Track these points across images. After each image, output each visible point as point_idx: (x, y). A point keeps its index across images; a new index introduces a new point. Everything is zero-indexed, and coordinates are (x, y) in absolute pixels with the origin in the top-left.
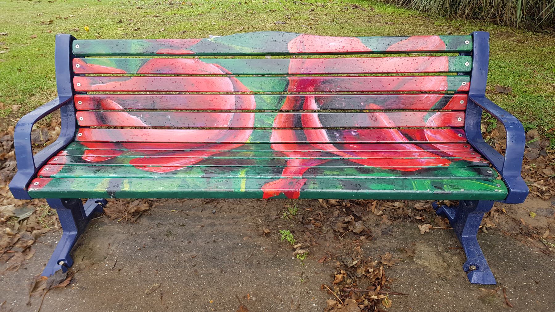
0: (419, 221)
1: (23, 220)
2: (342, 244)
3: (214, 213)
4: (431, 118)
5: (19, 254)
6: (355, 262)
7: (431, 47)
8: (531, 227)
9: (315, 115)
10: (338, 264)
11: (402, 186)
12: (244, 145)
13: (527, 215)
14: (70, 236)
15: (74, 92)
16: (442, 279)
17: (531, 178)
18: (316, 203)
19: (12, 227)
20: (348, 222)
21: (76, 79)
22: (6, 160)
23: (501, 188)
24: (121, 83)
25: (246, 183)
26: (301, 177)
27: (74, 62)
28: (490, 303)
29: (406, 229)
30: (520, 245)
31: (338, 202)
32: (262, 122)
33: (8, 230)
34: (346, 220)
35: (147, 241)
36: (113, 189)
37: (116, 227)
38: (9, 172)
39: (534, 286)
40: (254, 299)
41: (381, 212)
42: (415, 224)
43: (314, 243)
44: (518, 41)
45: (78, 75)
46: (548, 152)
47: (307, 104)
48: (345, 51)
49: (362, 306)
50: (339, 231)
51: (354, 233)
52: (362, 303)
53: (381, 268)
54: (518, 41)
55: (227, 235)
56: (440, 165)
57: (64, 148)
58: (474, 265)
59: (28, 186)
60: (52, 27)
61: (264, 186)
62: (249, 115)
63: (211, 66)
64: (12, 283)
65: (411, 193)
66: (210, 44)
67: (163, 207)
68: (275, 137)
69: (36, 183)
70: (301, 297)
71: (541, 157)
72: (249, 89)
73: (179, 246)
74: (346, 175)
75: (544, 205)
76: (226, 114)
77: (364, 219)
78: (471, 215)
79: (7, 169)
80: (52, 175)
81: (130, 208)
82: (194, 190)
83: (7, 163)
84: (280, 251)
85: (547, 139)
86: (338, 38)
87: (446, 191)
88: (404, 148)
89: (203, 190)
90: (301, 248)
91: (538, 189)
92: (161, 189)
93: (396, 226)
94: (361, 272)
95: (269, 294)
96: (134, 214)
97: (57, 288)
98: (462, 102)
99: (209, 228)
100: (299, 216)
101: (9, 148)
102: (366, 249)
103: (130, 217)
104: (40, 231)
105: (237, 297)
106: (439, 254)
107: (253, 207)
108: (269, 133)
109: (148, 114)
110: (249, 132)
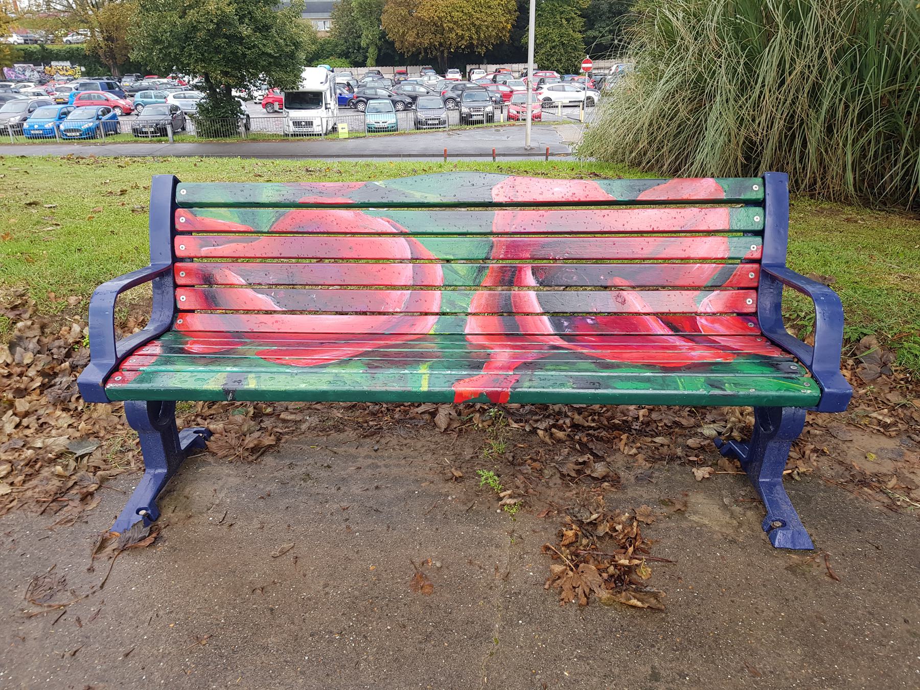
0: (693, 464)
1: (82, 456)
2: (574, 492)
3: (376, 451)
4: (706, 300)
5: (77, 503)
6: (595, 516)
7: (702, 196)
8: (868, 473)
9: (532, 294)
10: (568, 519)
11: (661, 385)
12: (423, 337)
13: (863, 458)
14: (155, 476)
15: (175, 259)
16: (730, 542)
17: (869, 405)
18: (534, 438)
19: (65, 467)
20: (584, 463)
21: (178, 239)
22: (56, 375)
23: (811, 387)
24: (245, 245)
25: (429, 380)
26: (511, 373)
27: (176, 214)
28: (804, 574)
29: (673, 474)
30: (852, 497)
31: (569, 436)
32: (452, 303)
33: (59, 469)
34: (581, 460)
35: (273, 487)
36: (232, 386)
37: (224, 468)
38: (60, 391)
39: (873, 553)
40: (438, 565)
41: (634, 451)
42: (688, 467)
43: (531, 491)
44: (848, 220)
45: (183, 233)
46: (893, 369)
47: (520, 278)
48: (576, 199)
49: (605, 575)
50: (568, 475)
51: (594, 478)
52: (606, 570)
53: (635, 524)
54: (848, 220)
55: (396, 480)
56: (719, 360)
57: (156, 337)
58: (779, 520)
59: (106, 380)
60: (125, 199)
61: (456, 383)
62: (433, 295)
63: (378, 220)
64: (65, 542)
65: (676, 395)
66: (377, 189)
67: (297, 442)
68: (472, 326)
69: (118, 378)
70: (510, 563)
71: (884, 376)
72: (434, 255)
73: (323, 494)
74: (580, 371)
75: (890, 444)
76: (399, 292)
77: (608, 460)
78: (771, 444)
79: (57, 387)
80: (141, 368)
81: (246, 441)
82: (352, 389)
83: (58, 380)
84: (479, 501)
85: (890, 349)
86: (565, 182)
87: (729, 392)
88: (668, 341)
89: (366, 388)
90: (510, 497)
91: (879, 421)
92: (303, 386)
93: (659, 470)
94: (603, 529)
95: (461, 559)
96: (254, 450)
97: (135, 548)
98: (752, 275)
99: (369, 471)
100: (507, 454)
101: (61, 357)
102: (611, 500)
103: (246, 454)
104: (107, 472)
105: (413, 563)
106: (725, 507)
107: (436, 443)
108: (463, 320)
109: (282, 291)
110: (432, 319)
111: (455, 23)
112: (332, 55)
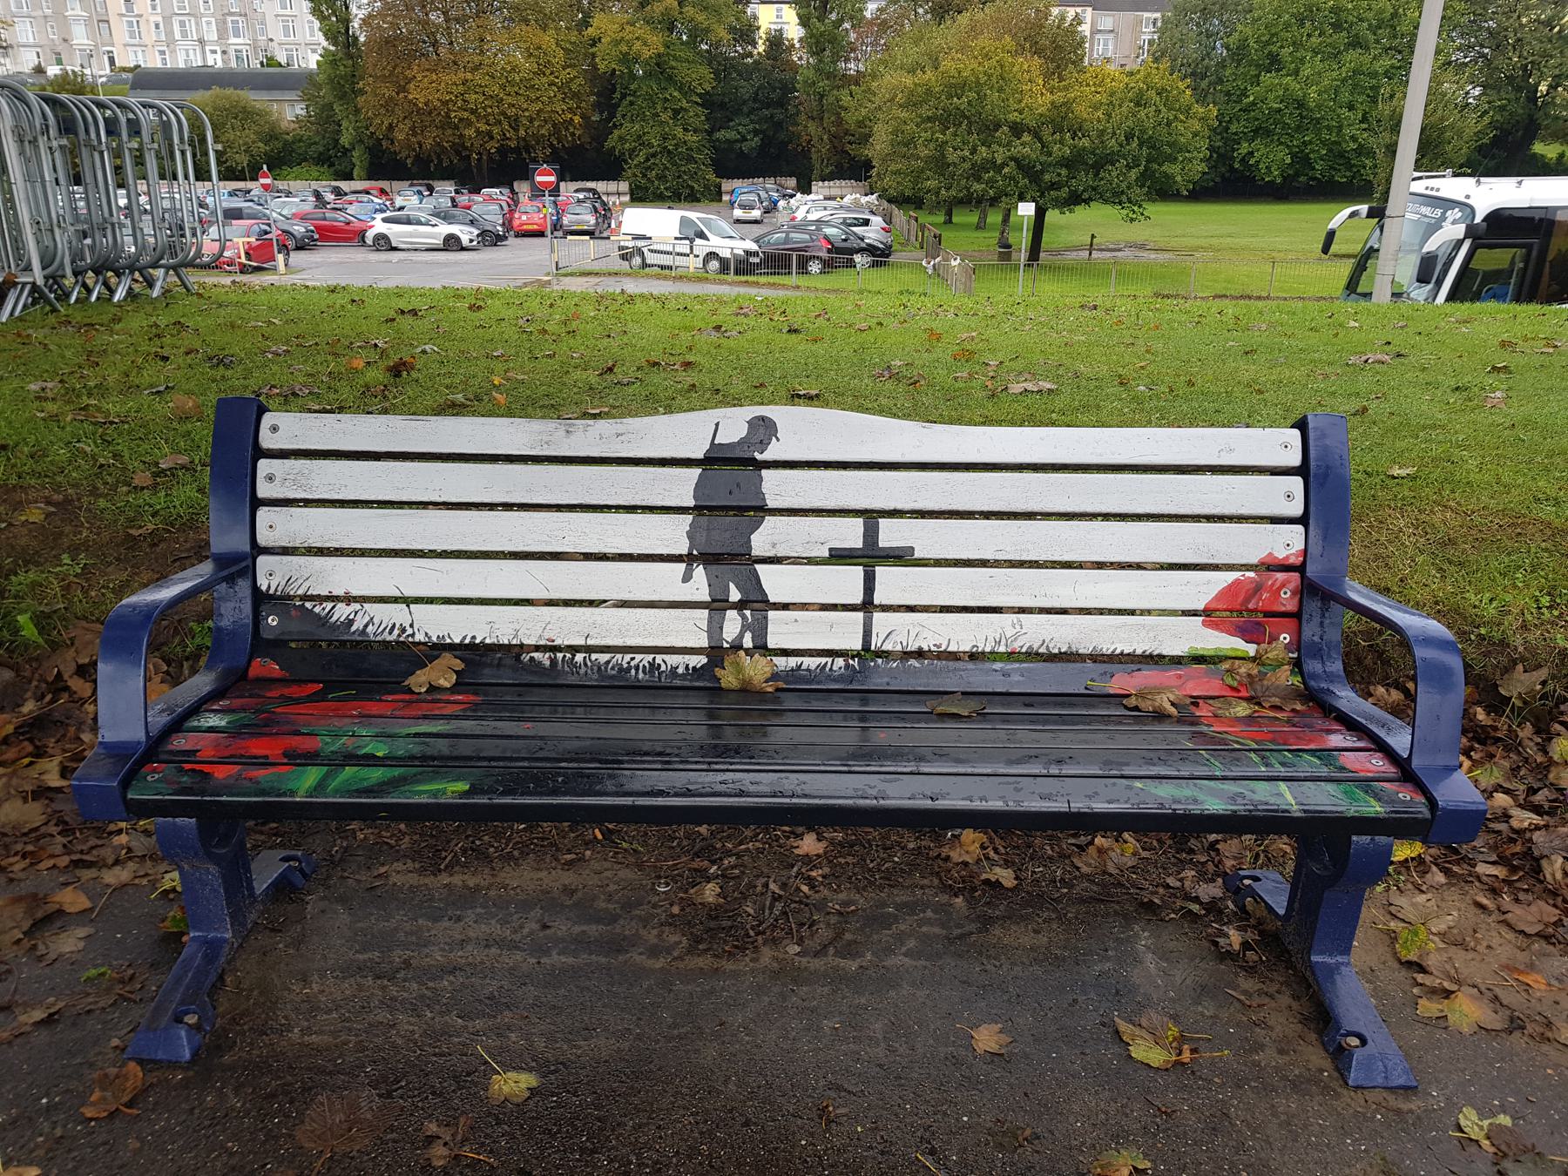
111: (473, 112)
112: (305, 160)
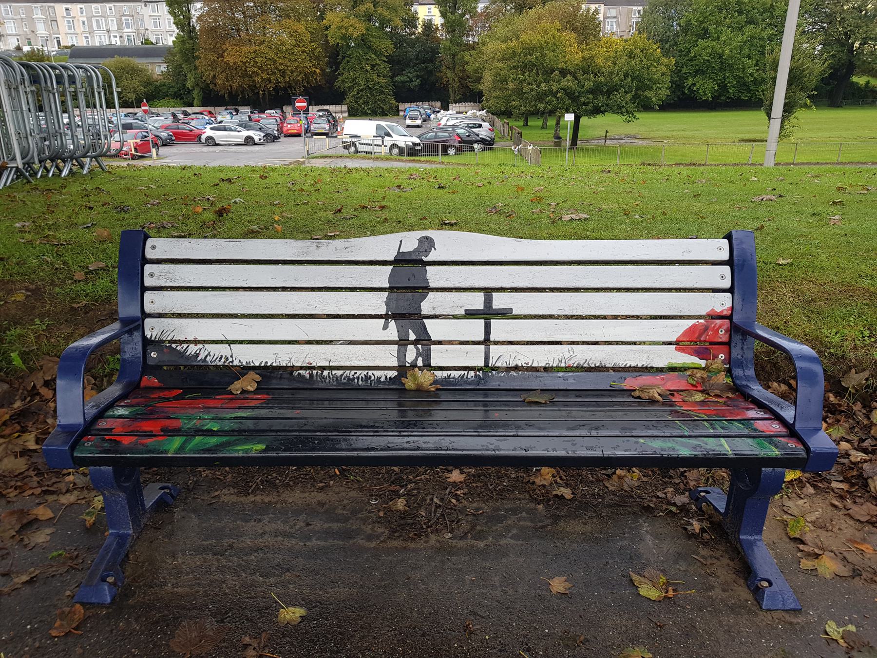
59: (73, 448)
112: (167, 96)
